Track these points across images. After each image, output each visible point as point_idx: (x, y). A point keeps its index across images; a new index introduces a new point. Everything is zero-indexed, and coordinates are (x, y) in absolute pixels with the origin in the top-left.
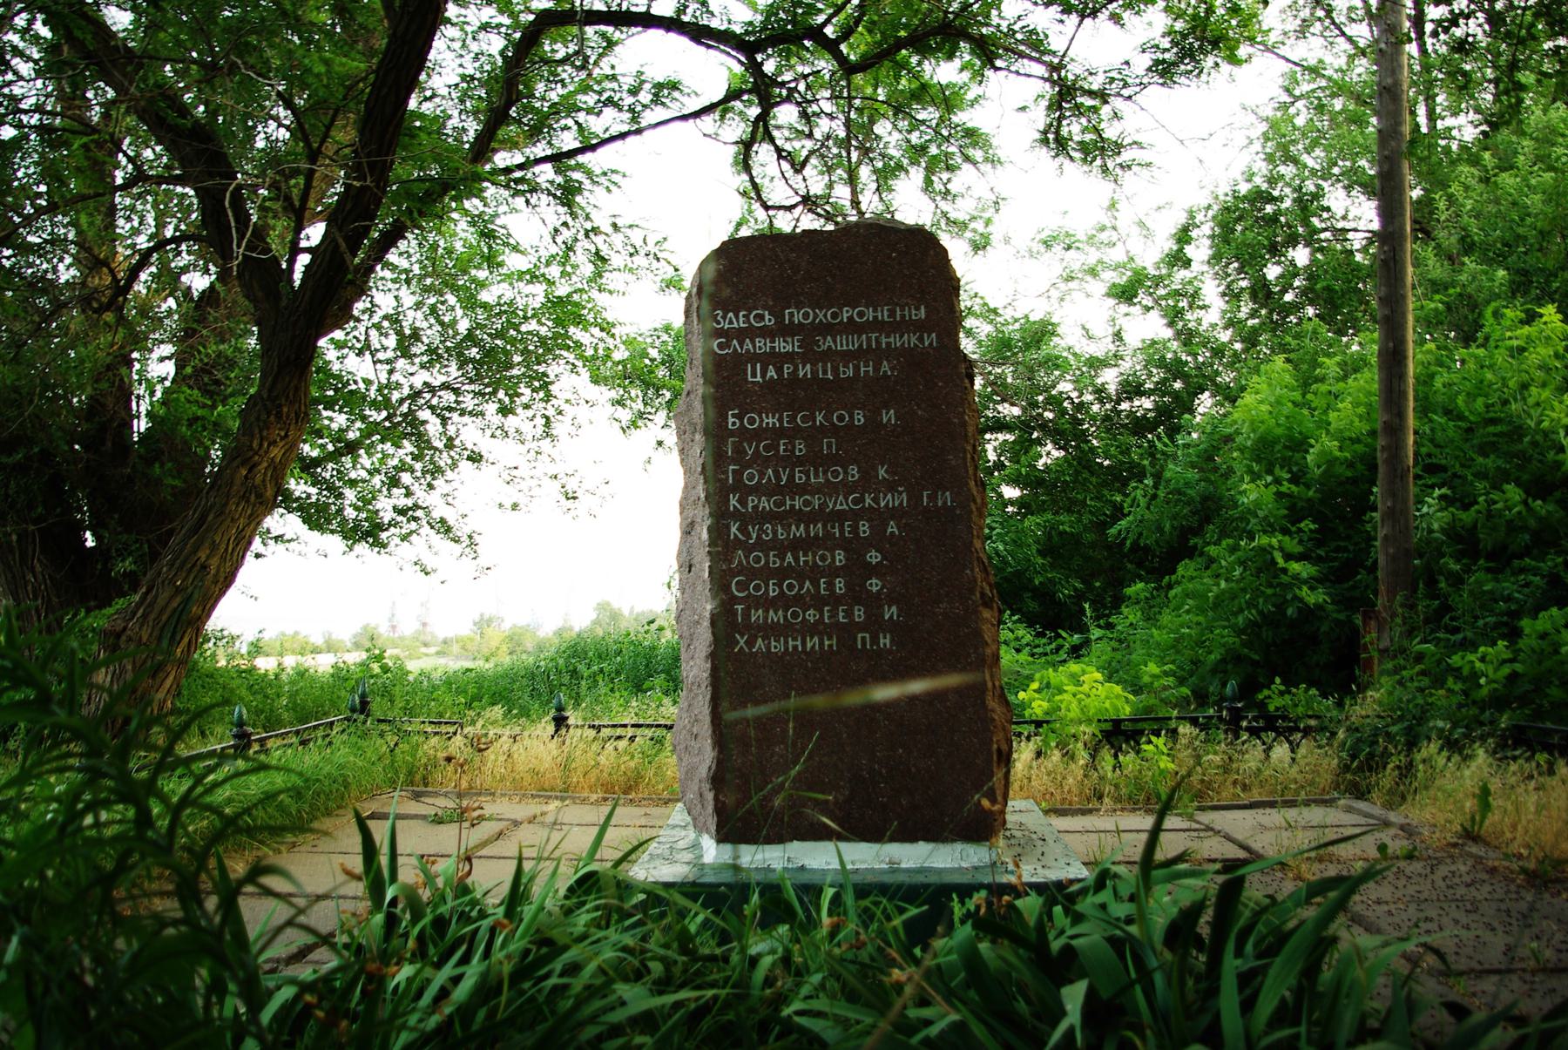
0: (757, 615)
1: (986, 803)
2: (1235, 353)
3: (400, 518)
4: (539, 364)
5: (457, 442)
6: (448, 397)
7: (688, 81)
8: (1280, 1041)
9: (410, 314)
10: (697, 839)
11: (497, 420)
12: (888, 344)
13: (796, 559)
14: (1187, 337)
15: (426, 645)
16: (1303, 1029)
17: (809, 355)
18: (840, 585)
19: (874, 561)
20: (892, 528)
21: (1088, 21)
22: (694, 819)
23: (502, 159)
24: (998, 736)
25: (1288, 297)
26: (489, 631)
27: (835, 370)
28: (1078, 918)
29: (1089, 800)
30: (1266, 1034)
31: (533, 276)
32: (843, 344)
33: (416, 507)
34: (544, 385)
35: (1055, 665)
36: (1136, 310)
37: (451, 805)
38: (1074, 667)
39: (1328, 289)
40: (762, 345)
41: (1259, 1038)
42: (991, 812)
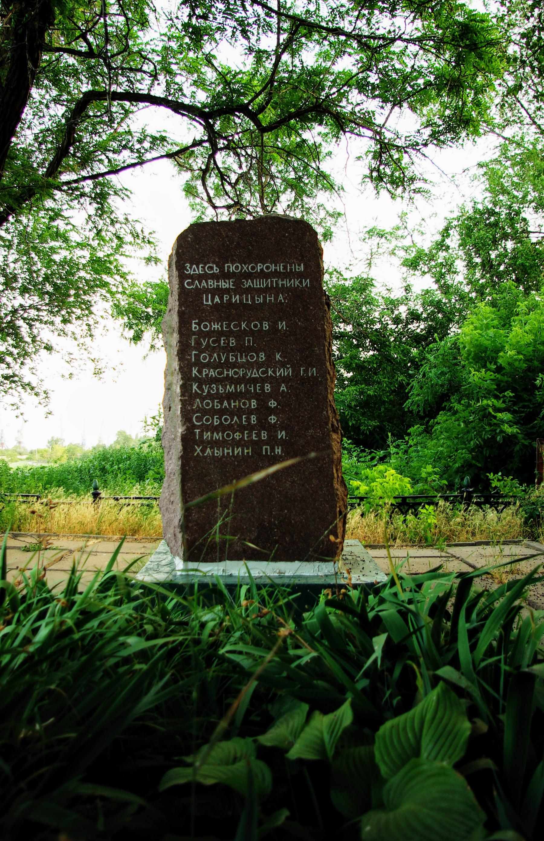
0: (207, 435)
1: (332, 538)
2: (471, 299)
3: (5, 381)
4: (85, 295)
5: (38, 339)
6: (33, 313)
7: (170, 136)
8: (490, 665)
9: (12, 265)
10: (172, 560)
11: (61, 326)
12: (283, 285)
13: (230, 404)
14: (446, 289)
15: (20, 454)
16: (502, 656)
17: (238, 290)
18: (253, 419)
19: (273, 406)
20: (283, 388)
21: (396, 109)
22: (171, 549)
23: (65, 178)
24: (340, 504)
25: (502, 268)
26: (56, 447)
27: (253, 299)
28: (382, 601)
29: (388, 540)
30: (483, 660)
31: (81, 246)
32: (258, 284)
33: (14, 375)
34: (88, 306)
35: (371, 467)
36: (418, 273)
37: (35, 541)
38: (381, 467)
39: (522, 264)
40: (212, 284)
41: (479, 664)
42: (335, 543)
